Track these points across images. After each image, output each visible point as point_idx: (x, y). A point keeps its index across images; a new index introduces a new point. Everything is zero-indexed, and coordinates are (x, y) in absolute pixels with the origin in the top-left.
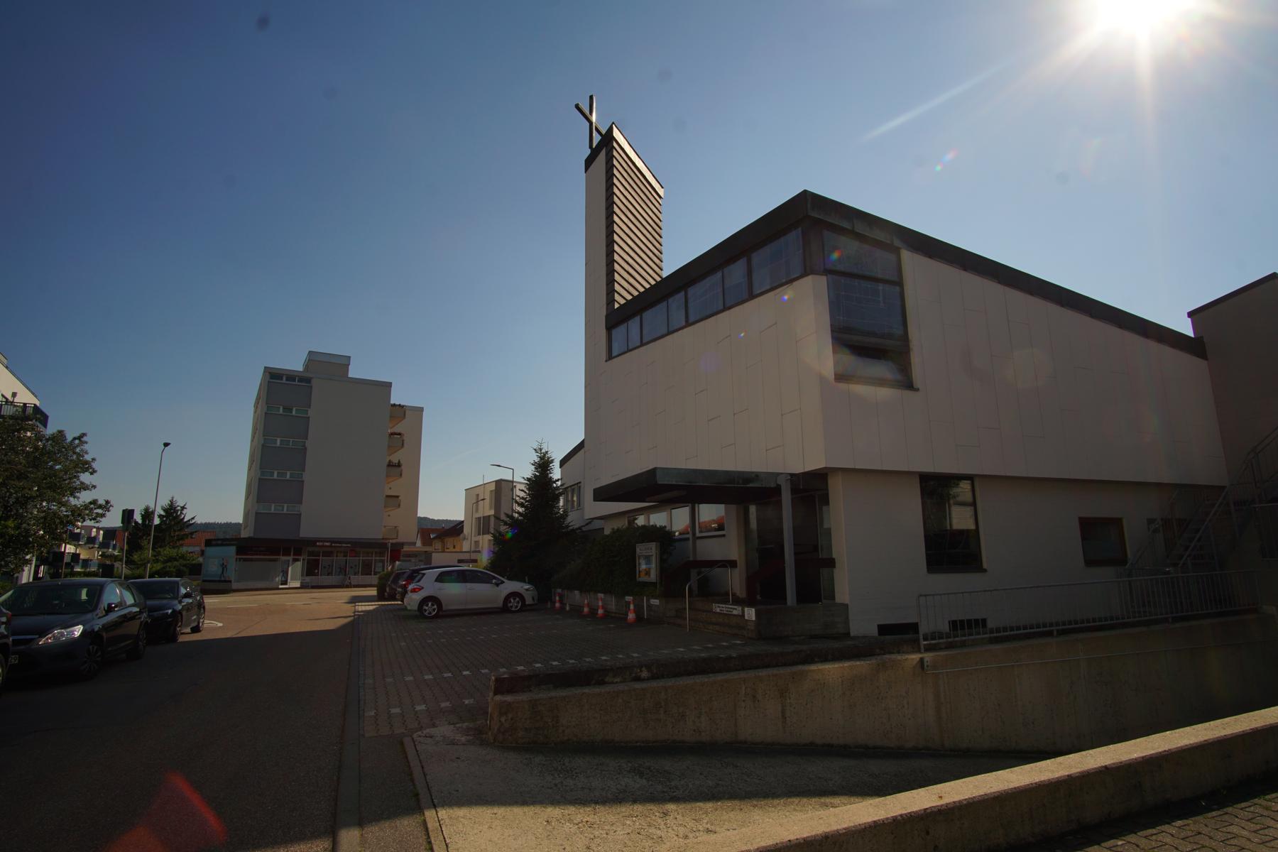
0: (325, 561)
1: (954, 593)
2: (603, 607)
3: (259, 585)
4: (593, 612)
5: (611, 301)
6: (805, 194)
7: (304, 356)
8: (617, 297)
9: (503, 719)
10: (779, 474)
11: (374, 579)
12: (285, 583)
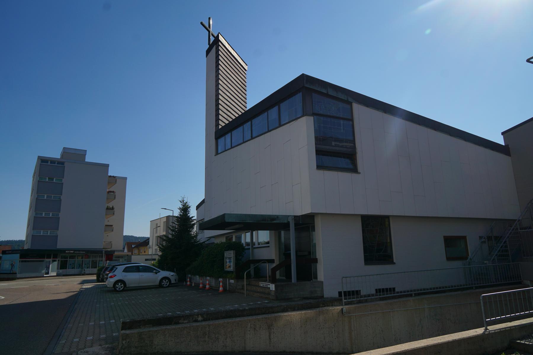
0: (69, 261)
1: (378, 276)
2: (209, 284)
3: (27, 275)
4: (204, 287)
5: (217, 124)
6: (303, 75)
7: (60, 151)
8: (220, 122)
9: (124, 342)
10: (289, 216)
11: (95, 270)
12: (48, 273)
